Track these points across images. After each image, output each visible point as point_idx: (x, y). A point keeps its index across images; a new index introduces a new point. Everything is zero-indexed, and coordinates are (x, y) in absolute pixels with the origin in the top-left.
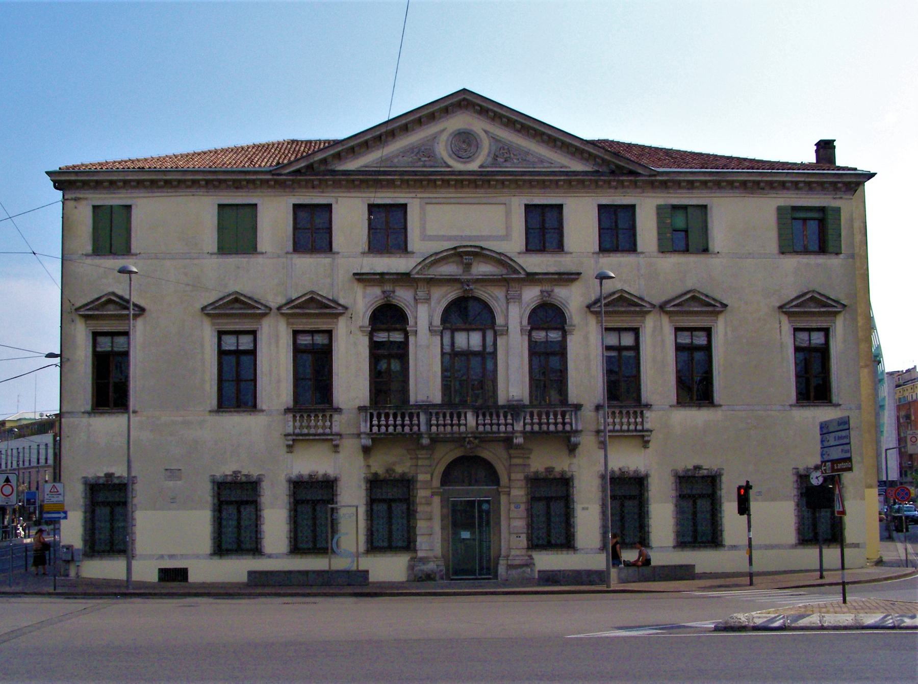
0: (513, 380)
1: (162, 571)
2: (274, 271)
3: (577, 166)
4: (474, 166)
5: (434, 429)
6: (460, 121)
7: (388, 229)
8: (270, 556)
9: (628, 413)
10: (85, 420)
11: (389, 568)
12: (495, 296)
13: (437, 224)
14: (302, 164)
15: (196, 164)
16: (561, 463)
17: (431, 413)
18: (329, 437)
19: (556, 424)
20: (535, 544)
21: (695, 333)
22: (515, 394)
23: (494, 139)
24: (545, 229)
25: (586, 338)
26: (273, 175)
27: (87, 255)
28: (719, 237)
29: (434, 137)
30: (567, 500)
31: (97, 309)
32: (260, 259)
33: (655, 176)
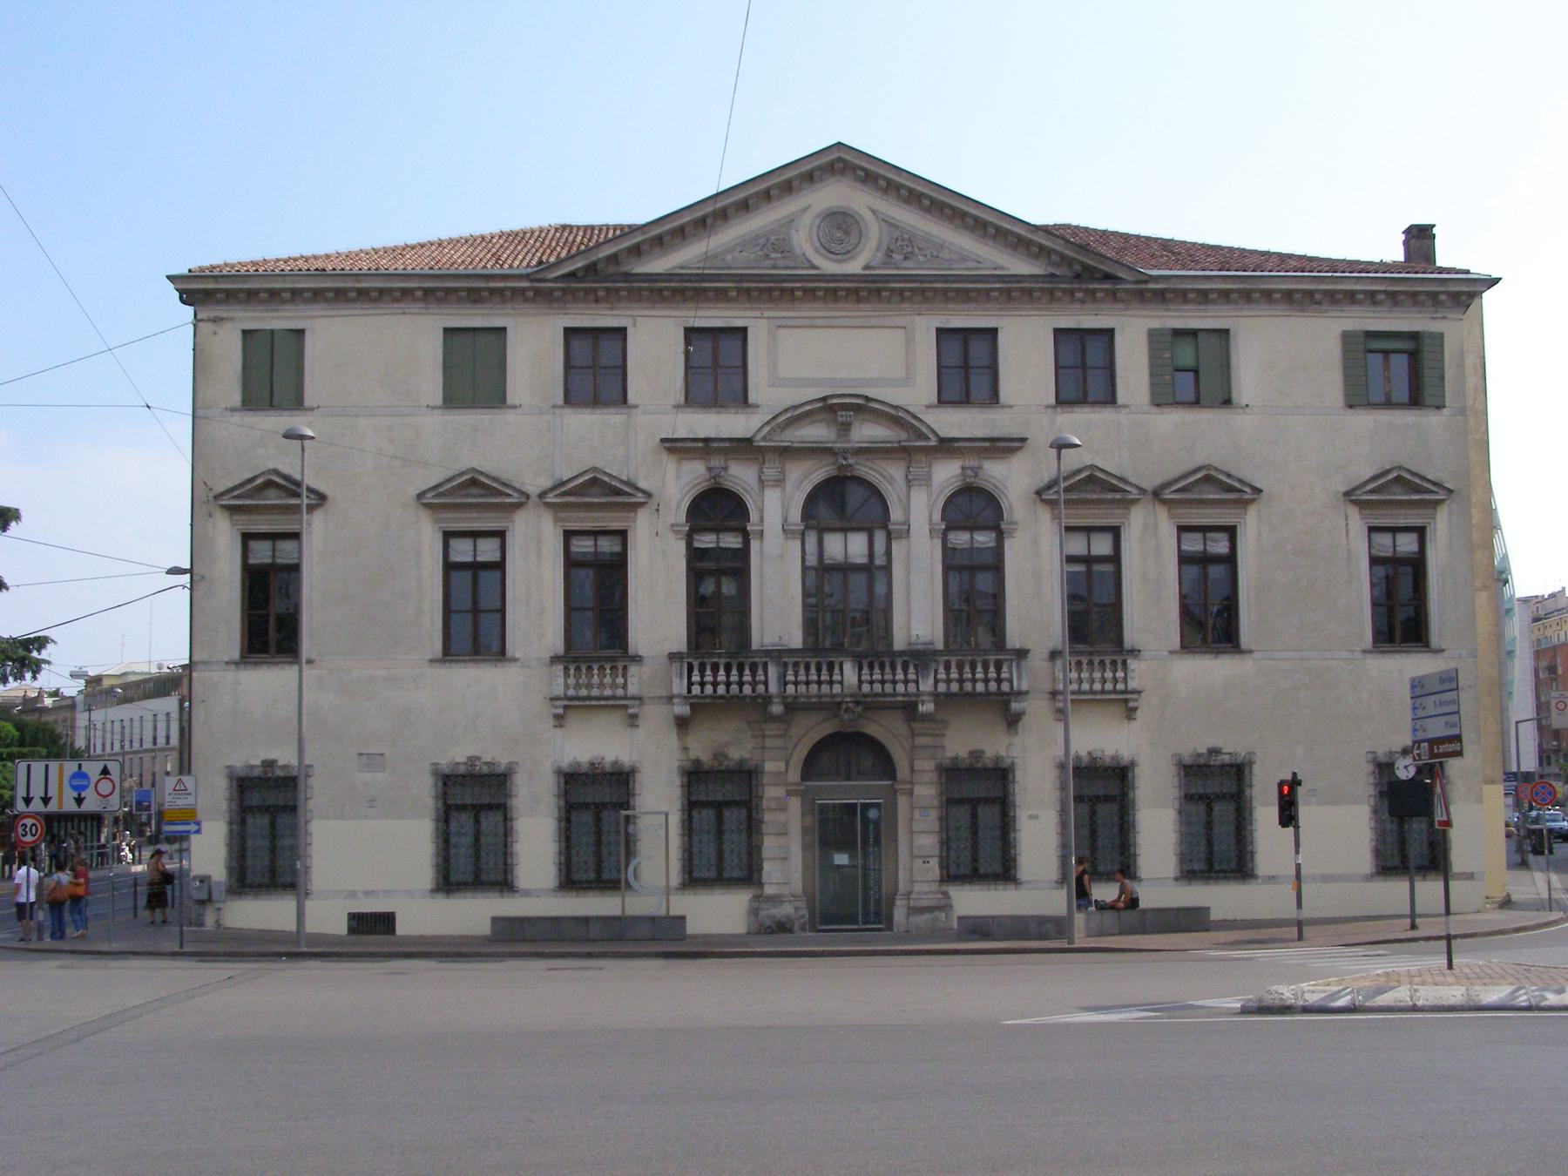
0: (918, 613)
2: (533, 436)
3: (1020, 266)
4: (854, 267)
5: (791, 689)
8: (527, 893)
9: (1102, 663)
10: (231, 675)
11: (718, 912)
12: (889, 477)
13: (797, 359)
14: (580, 264)
16: (993, 743)
19: (986, 681)
20: (952, 875)
24: (968, 367)
27: (233, 410)
28: (1248, 378)
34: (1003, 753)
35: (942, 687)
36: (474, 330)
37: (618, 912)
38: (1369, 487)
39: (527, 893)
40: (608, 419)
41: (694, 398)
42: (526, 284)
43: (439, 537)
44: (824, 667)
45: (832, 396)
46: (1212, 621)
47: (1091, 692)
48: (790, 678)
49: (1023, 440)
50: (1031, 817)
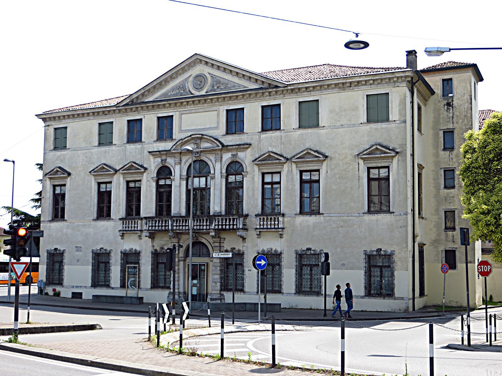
0: (217, 203)
1: (73, 293)
2: (119, 153)
3: (253, 86)
4: (203, 93)
5: (175, 228)
6: (199, 69)
7: (165, 127)
8: (113, 288)
9: (271, 219)
10: (49, 224)
11: (161, 297)
12: (210, 159)
13: (187, 122)
14: (128, 101)
15: (99, 105)
16: (239, 246)
17: (174, 220)
18: (136, 232)
19: (230, 225)
20: (225, 287)
21: (274, 175)
22: (217, 210)
23: (212, 76)
24: (235, 121)
25: (253, 178)
26: (117, 107)
27: (52, 150)
28: (324, 118)
29: (187, 79)
30: (107, 264)
31: (54, 175)
32: (113, 148)
33: (286, 87)
34: (241, 249)
35: (216, 227)
36: (377, 94)
37: (125, 295)
38: (365, 153)
39: (113, 288)
40: (138, 146)
41: (160, 138)
42: (115, 108)
43: (96, 184)
44: (184, 221)
45: (192, 135)
46: (309, 205)
47: (267, 228)
48: (175, 224)
49: (250, 145)
50: (249, 270)
